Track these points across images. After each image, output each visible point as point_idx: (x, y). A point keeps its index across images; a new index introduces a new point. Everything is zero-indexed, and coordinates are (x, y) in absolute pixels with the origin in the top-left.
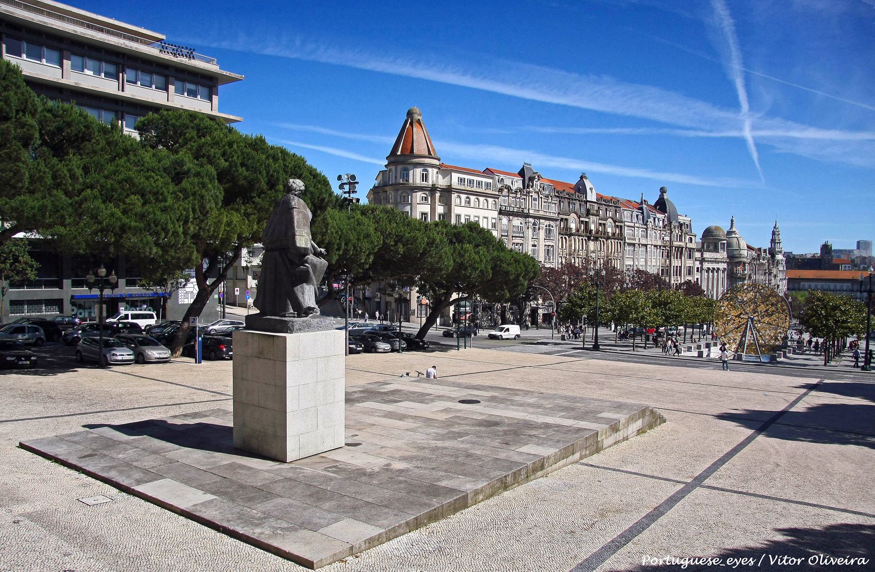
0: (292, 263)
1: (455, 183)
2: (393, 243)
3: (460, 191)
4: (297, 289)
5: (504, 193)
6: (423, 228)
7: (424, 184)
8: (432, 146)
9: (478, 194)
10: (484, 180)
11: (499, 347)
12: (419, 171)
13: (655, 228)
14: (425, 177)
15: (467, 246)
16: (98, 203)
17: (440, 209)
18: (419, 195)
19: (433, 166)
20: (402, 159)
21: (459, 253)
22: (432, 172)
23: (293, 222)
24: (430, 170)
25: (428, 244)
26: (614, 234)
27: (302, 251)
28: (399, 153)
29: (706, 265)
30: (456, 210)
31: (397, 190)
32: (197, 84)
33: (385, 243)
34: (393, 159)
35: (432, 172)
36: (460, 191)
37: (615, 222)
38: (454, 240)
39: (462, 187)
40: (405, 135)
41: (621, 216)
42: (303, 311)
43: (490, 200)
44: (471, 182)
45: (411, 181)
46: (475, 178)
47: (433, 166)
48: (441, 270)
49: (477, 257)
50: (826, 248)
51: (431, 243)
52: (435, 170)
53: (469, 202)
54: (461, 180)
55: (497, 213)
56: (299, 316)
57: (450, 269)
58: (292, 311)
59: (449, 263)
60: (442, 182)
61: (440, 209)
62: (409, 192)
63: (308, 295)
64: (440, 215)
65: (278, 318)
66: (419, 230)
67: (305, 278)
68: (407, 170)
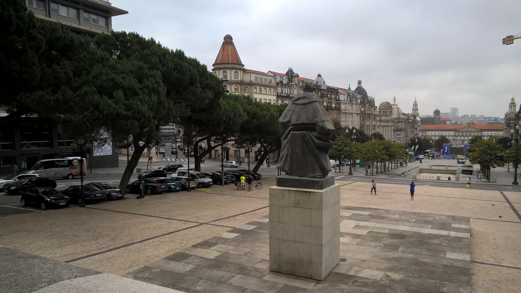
9: (265, 86)
11: (511, 190)
13: (356, 104)
16: (96, 97)
26: (336, 108)
29: (383, 124)
32: (98, 15)
37: (336, 100)
41: (339, 97)
43: (272, 90)
50: (437, 112)
53: (261, 91)
65: (297, 178)
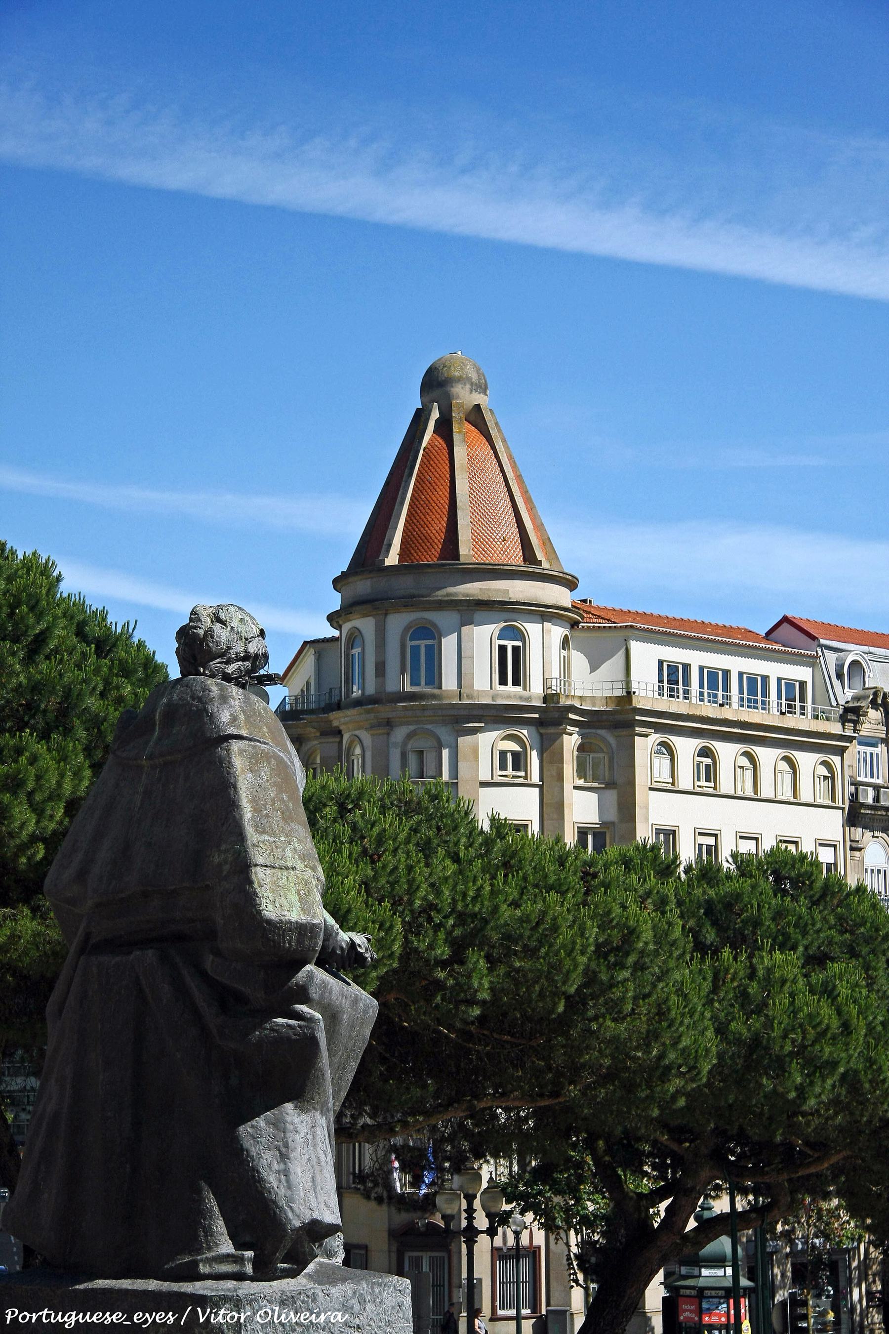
0: (227, 1000)
1: (646, 689)
2: (443, 951)
3: (670, 725)
4: (244, 1130)
5: (866, 729)
6: (574, 879)
7: (510, 693)
8: (539, 527)
9: (749, 735)
10: (774, 670)
12: (483, 637)
14: (511, 665)
15: (785, 963)
17: (583, 808)
18: (488, 743)
19: (545, 613)
20: (405, 584)
21: (743, 995)
22: (543, 642)
23: (233, 805)
24: (533, 629)
25: (602, 951)
27: (291, 942)
28: (392, 559)
30: (655, 812)
31: (389, 724)
33: (409, 953)
34: (362, 586)
35: (543, 642)
36: (670, 725)
38: (710, 935)
39: (678, 706)
40: (417, 480)
42: (277, 1246)
43: (807, 761)
44: (715, 680)
45: (449, 682)
46: (736, 664)
47: (545, 613)
48: (665, 1074)
49: (826, 1011)
51: (617, 948)
52: (557, 632)
53: (711, 774)
54: (672, 676)
55: (837, 817)
56: (264, 1271)
57: (706, 1068)
58: (227, 1247)
59: (699, 1041)
60: (590, 686)
61: (583, 808)
62: (443, 733)
63: (302, 1160)
64: (582, 833)
66: (560, 889)
67: (286, 1076)
68: (430, 634)
